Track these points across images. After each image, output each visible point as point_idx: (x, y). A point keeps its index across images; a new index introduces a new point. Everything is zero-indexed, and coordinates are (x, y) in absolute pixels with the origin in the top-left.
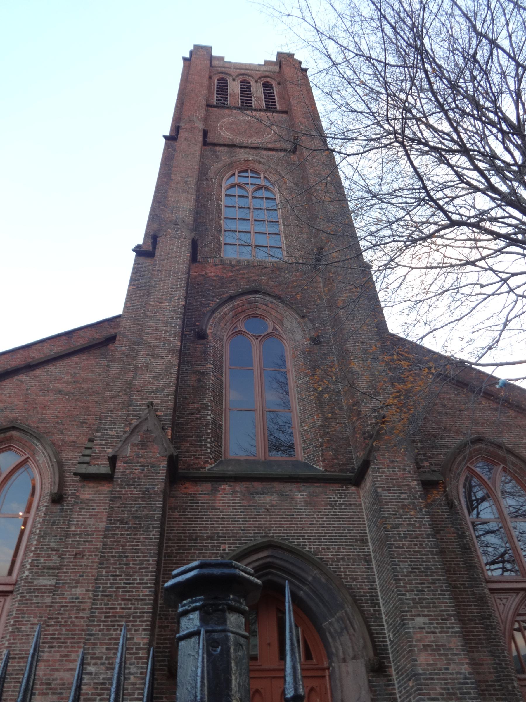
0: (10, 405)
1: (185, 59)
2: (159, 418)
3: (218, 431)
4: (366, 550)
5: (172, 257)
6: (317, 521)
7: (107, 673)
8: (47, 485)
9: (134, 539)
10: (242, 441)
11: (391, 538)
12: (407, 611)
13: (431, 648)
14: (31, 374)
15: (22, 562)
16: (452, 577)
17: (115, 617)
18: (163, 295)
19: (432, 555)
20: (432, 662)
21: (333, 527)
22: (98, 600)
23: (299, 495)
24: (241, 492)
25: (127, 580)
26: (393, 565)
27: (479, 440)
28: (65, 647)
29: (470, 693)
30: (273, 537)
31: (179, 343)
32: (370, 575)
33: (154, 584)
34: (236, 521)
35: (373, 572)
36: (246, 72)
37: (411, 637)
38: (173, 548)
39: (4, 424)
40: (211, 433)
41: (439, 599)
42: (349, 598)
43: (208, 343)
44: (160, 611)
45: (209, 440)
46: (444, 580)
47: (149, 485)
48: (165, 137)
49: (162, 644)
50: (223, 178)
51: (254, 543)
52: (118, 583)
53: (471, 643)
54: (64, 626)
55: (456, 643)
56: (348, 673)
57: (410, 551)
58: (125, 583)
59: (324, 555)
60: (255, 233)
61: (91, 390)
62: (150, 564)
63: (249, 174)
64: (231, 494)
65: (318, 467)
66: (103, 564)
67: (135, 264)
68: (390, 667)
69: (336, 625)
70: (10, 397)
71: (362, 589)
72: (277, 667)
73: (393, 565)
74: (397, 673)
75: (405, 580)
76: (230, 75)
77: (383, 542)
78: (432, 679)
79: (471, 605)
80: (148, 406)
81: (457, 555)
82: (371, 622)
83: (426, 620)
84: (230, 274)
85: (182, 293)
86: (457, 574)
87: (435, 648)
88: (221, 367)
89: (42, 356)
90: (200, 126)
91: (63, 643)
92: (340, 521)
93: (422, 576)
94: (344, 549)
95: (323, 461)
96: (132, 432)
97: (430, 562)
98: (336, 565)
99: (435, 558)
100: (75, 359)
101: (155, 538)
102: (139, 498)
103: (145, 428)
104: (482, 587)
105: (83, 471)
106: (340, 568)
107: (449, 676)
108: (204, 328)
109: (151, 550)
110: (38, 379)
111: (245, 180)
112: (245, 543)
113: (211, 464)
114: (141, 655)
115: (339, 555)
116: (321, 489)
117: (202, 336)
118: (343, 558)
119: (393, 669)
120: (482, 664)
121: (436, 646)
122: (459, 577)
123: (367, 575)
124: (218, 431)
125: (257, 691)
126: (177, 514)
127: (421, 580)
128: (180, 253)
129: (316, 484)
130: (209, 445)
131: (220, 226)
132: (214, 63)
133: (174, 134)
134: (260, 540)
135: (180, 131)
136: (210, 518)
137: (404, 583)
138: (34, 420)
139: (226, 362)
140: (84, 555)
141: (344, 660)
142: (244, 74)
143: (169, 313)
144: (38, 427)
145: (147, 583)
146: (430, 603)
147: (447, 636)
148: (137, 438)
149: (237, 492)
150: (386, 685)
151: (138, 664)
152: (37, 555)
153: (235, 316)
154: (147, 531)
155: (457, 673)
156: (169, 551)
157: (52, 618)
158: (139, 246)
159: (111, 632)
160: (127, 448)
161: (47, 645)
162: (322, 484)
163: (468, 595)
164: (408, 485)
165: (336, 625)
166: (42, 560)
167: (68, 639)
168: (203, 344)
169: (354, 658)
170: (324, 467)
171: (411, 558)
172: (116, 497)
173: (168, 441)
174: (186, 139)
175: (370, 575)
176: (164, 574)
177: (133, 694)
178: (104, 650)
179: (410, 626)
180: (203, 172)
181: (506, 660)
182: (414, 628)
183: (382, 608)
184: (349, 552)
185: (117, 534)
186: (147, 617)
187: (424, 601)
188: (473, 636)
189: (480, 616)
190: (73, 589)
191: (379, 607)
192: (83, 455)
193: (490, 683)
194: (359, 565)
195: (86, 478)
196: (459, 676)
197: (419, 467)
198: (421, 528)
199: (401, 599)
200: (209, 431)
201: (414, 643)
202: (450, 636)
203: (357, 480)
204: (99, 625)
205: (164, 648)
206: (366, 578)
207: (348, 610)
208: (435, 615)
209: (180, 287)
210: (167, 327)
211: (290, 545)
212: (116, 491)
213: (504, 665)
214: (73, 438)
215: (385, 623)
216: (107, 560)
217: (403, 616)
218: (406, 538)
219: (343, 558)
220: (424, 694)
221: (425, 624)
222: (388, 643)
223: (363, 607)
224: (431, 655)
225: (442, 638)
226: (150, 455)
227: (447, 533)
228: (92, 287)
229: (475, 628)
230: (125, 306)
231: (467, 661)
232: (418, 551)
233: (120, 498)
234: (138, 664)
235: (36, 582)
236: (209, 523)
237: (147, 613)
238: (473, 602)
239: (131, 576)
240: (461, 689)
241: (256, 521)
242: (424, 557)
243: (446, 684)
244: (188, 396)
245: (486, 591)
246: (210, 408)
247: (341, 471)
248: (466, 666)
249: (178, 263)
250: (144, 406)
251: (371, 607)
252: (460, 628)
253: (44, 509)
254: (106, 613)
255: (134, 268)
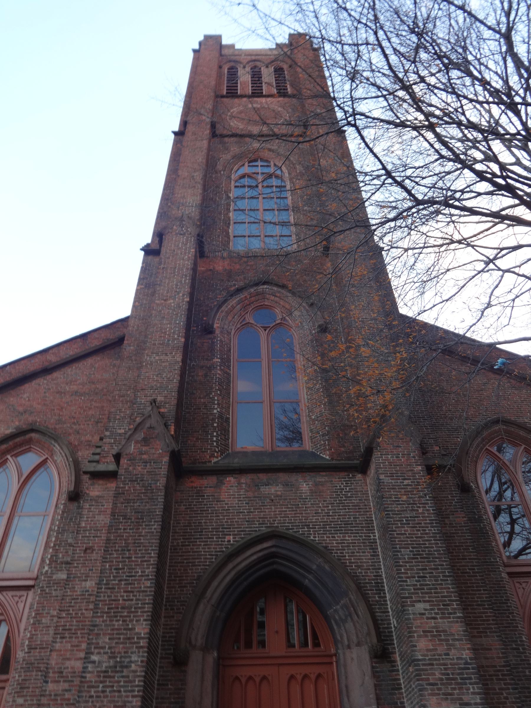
0: (29, 409)
1: (195, 51)
2: (162, 415)
3: (225, 424)
4: (372, 537)
5: (177, 254)
6: (322, 510)
7: (109, 662)
8: (65, 483)
9: (137, 533)
10: (250, 435)
11: (393, 524)
12: (407, 598)
13: (434, 633)
14: (49, 377)
15: (42, 558)
16: (461, 562)
17: (118, 608)
18: (168, 293)
19: (434, 540)
20: (432, 647)
21: (339, 515)
22: (102, 592)
23: (305, 485)
24: (246, 484)
25: (130, 572)
26: (394, 552)
27: (497, 422)
28: (76, 638)
29: (470, 679)
30: (277, 527)
31: (183, 340)
32: (375, 562)
33: (155, 576)
34: (241, 512)
35: (379, 559)
36: (257, 57)
37: (412, 624)
38: (179, 541)
39: (24, 427)
40: (218, 426)
41: (442, 584)
42: (353, 585)
43: (215, 338)
44: (166, 602)
45: (215, 434)
46: (447, 565)
47: (152, 480)
48: (175, 133)
49: (168, 633)
50: (232, 169)
51: (258, 534)
52: (120, 576)
53: (479, 628)
54: (75, 618)
55: (458, 628)
56: (352, 659)
57: (412, 538)
58: (127, 576)
59: (329, 543)
60: (261, 224)
61: (105, 390)
62: (151, 557)
63: (259, 163)
64: (237, 486)
65: (324, 456)
66: (106, 558)
67: (143, 263)
68: (395, 653)
69: (341, 613)
70: (29, 400)
71: (367, 576)
72: (284, 654)
73: (394, 552)
74: (401, 659)
75: (406, 566)
76: (240, 63)
77: (385, 529)
78: (432, 665)
79: (480, 590)
80: (151, 404)
81: (467, 539)
82: (375, 608)
83: (427, 606)
84: (238, 267)
85: (187, 289)
86: (466, 559)
87: (435, 633)
88: (229, 360)
89: (59, 359)
90: (207, 119)
91: (74, 634)
92: (345, 509)
93: (424, 562)
94: (349, 536)
95: (330, 449)
96: (136, 429)
97: (433, 547)
98: (341, 553)
99: (438, 544)
100: (90, 361)
101: (157, 532)
102: (142, 493)
103: (148, 425)
104: (500, 571)
105: (92, 469)
106: (345, 556)
107: (449, 662)
108: (211, 323)
109: (152, 543)
110: (55, 382)
111: (254, 170)
112: (250, 534)
113: (217, 457)
114: (142, 644)
115: (344, 543)
116: (326, 478)
117: (209, 330)
118: (348, 546)
119: (397, 655)
120: (491, 649)
121: (437, 631)
122: (468, 562)
123: (372, 562)
124: (225, 424)
125: (264, 678)
126: (183, 508)
127: (422, 566)
128: (186, 249)
129: (321, 473)
130: (215, 439)
131: (229, 219)
132: (225, 52)
133: (183, 129)
134: (264, 530)
135: (188, 126)
136: (216, 510)
137: (405, 570)
138: (52, 421)
139: (234, 355)
140: (93, 550)
141: (349, 647)
142: (255, 61)
143: (174, 310)
144: (55, 428)
145: (148, 576)
146: (431, 589)
147: (448, 622)
148: (140, 436)
149: (243, 483)
150: (390, 671)
151: (139, 652)
152: (56, 551)
153: (245, 307)
154: (149, 525)
155: (458, 659)
156: (175, 544)
157: (64, 611)
158: (148, 245)
159: (114, 623)
160: (131, 445)
161: (59, 636)
162: (327, 473)
163: (477, 580)
164: (412, 470)
165: (341, 613)
166: (61, 556)
167: (79, 629)
168: (210, 339)
169: (359, 644)
170: (330, 455)
171: (413, 544)
172: (120, 494)
173: (171, 438)
174: (194, 134)
175: (375, 562)
176: (169, 566)
177: (135, 681)
178: (107, 640)
179: (410, 612)
180: (210, 165)
181: (524, 645)
182: (414, 614)
183: (387, 595)
184: (355, 540)
185: (120, 529)
186: (148, 608)
187: (425, 587)
188: (481, 620)
189: (489, 601)
190: (84, 583)
191: (385, 593)
192: (94, 454)
193: (499, 668)
194: (365, 552)
195: (96, 476)
196: (459, 661)
197: (424, 451)
198: (425, 513)
199: (401, 586)
200: (215, 425)
201: (414, 629)
202: (451, 622)
203: (363, 468)
204: (103, 617)
205: (170, 637)
206: (372, 566)
207: (352, 597)
208: (436, 601)
209: (185, 283)
210: (172, 325)
211: (294, 534)
212: (119, 488)
213: (521, 650)
214: (88, 437)
215: (390, 610)
216: (111, 554)
217: (403, 602)
218: (409, 524)
219: (348, 546)
220: (422, 680)
221: (426, 610)
222: (393, 629)
223: (368, 594)
224: (431, 640)
225: (443, 623)
226: (153, 451)
227: (456, 517)
228: (100, 289)
229: (484, 613)
230: (134, 306)
231: (469, 646)
232: (420, 537)
233: (124, 494)
234: (139, 652)
235: (54, 577)
236: (214, 515)
237: (148, 604)
238: (482, 587)
239: (133, 569)
240: (462, 674)
241: (261, 512)
242: (427, 543)
243: (445, 669)
244: (195, 392)
245: (504, 575)
246: (216, 402)
247: (349, 459)
248: (467, 651)
249: (183, 259)
250: (148, 404)
251: (376, 594)
252: (462, 613)
253: (62, 507)
254: (109, 604)
255: (142, 267)
